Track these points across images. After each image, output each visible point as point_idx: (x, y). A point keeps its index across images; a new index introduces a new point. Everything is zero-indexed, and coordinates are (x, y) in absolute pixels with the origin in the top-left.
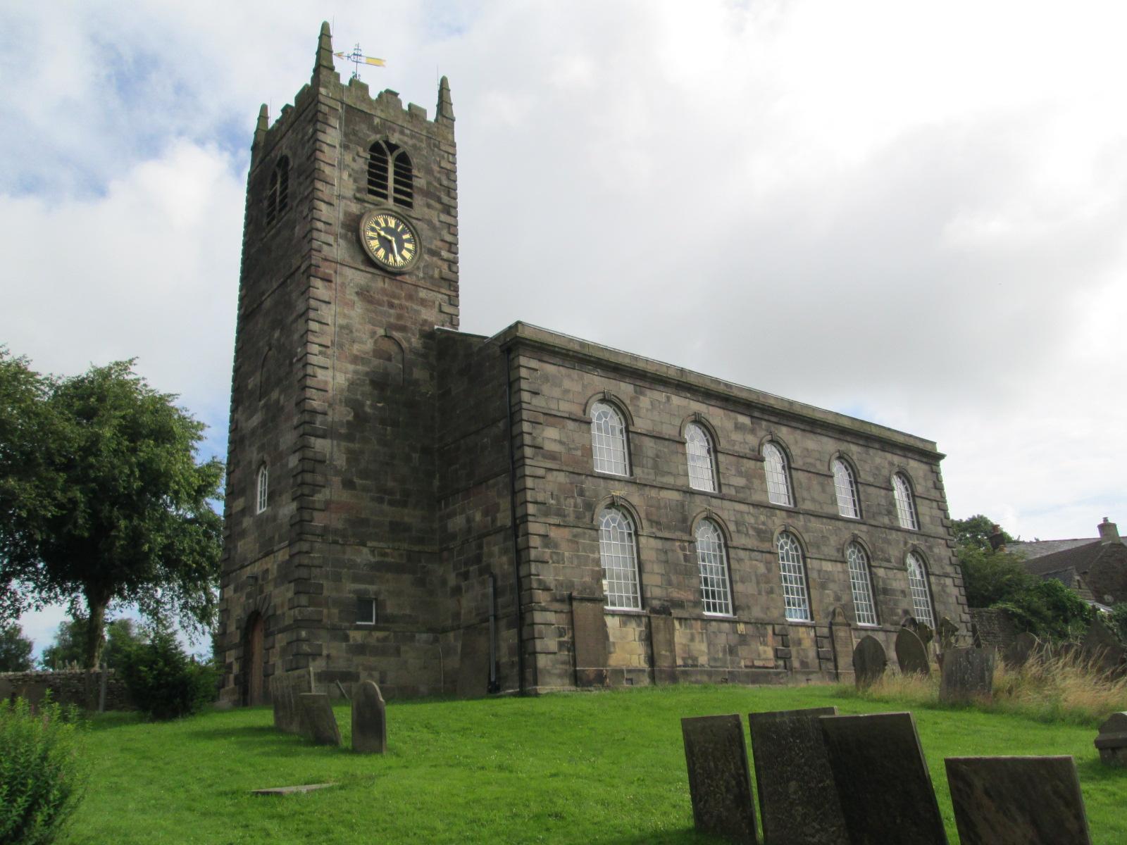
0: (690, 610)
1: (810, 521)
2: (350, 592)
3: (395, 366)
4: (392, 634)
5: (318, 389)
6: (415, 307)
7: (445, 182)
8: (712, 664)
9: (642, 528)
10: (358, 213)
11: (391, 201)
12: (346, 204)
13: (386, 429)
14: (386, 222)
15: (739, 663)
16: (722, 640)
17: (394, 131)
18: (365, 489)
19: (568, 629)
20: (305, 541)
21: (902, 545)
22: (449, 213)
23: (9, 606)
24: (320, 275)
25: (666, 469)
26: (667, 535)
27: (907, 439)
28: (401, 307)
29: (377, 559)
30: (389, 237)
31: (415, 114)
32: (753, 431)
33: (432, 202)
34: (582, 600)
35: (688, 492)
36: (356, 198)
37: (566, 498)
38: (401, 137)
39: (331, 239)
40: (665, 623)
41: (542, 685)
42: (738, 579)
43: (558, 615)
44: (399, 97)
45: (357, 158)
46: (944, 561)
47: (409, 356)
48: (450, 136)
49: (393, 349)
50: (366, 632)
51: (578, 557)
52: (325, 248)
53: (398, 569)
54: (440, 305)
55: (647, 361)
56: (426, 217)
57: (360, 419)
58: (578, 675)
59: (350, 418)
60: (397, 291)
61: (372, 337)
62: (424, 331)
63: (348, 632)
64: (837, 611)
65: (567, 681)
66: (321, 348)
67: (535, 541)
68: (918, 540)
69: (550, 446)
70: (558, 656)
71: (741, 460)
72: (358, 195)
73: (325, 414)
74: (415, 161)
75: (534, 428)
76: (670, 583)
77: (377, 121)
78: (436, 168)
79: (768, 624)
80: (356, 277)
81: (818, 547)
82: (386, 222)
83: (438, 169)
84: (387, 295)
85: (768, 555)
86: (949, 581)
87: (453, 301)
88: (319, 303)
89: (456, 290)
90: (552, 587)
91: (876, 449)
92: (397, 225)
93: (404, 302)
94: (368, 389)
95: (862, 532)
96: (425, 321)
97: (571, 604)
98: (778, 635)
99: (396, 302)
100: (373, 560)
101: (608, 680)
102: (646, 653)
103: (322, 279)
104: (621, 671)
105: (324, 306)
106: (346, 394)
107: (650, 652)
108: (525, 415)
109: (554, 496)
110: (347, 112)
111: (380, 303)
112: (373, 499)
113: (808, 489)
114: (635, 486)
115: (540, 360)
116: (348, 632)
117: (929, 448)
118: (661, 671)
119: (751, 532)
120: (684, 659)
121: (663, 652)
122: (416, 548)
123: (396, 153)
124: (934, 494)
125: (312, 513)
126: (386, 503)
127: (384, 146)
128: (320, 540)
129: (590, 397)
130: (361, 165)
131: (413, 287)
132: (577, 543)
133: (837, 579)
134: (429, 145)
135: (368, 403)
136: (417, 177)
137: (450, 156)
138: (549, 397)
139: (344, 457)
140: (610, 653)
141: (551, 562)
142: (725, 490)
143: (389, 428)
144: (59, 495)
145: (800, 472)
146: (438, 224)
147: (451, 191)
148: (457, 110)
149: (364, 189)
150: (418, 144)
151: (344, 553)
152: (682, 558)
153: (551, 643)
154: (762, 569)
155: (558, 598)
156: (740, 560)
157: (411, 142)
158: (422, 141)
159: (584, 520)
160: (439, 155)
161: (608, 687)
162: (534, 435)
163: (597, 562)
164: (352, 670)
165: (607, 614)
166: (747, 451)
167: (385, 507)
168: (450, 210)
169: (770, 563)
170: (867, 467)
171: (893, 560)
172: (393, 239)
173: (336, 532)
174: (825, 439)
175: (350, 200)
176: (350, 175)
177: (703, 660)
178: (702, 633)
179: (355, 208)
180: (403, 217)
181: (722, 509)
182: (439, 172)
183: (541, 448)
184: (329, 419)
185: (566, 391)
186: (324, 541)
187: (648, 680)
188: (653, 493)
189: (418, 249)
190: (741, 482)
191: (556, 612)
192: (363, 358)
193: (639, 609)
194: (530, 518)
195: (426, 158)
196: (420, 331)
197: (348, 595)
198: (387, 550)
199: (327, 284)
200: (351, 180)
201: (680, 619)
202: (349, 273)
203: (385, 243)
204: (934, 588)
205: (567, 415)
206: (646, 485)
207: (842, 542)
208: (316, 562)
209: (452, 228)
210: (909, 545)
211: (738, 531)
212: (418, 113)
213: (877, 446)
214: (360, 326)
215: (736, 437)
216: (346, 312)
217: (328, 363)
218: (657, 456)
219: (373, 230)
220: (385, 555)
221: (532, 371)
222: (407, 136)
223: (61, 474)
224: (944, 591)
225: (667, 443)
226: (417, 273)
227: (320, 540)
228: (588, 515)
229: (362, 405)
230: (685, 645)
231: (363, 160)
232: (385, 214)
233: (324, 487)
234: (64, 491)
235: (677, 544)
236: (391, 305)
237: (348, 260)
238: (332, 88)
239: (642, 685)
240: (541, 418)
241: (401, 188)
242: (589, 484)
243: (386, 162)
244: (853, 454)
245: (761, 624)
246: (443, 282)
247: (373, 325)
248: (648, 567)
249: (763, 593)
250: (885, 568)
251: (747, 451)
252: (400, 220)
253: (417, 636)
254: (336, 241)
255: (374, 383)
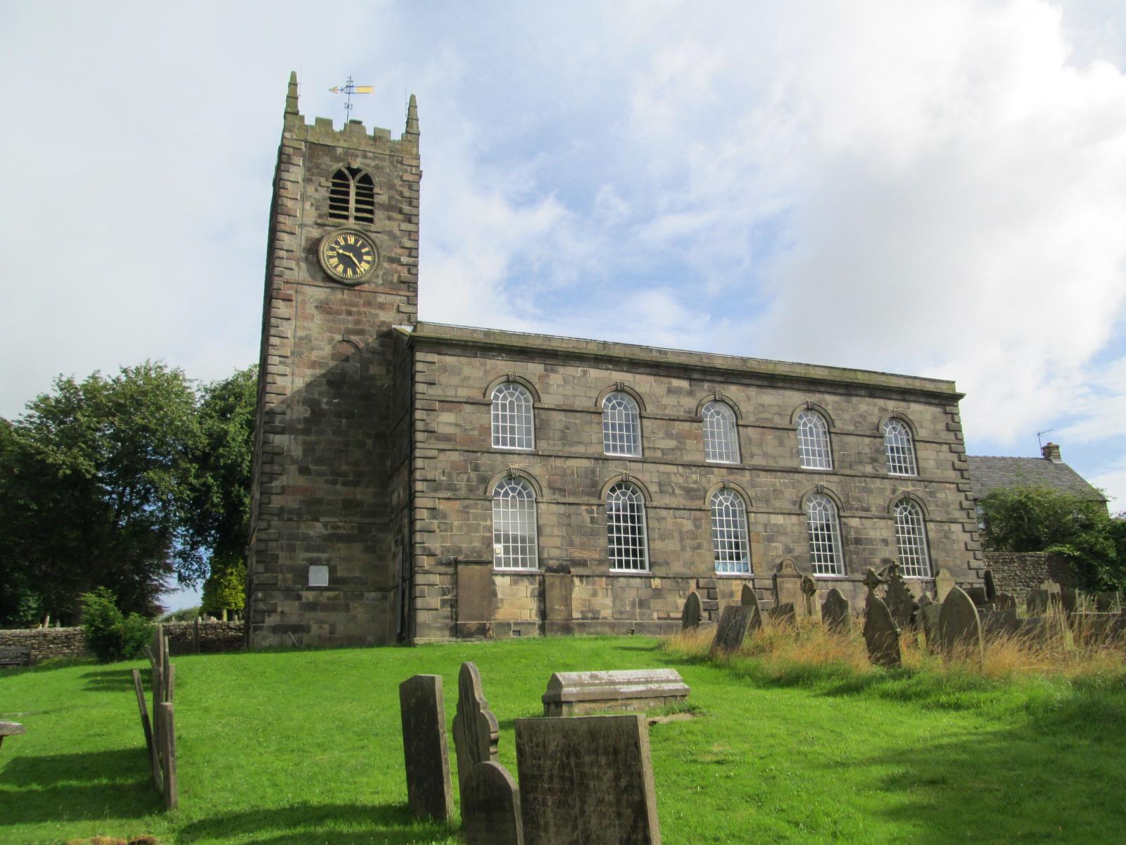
0: (594, 568)
1: (758, 476)
2: (303, 560)
3: (354, 365)
4: (342, 594)
5: (277, 394)
6: (373, 311)
7: (407, 193)
8: (618, 617)
9: (542, 496)
10: (319, 237)
11: (352, 221)
12: (308, 231)
13: (341, 422)
14: (346, 240)
15: (652, 615)
16: (631, 595)
17: (357, 156)
18: (321, 474)
19: (453, 588)
20: (263, 520)
21: (888, 493)
22: (410, 221)
23: (196, 569)
24: (280, 296)
25: (575, 439)
26: (571, 500)
27: (910, 381)
28: (359, 313)
29: (330, 531)
30: (347, 254)
31: (379, 137)
32: (691, 393)
33: (394, 215)
34: (467, 563)
35: (601, 459)
36: (317, 224)
37: (458, 475)
38: (363, 161)
39: (293, 264)
40: (561, 581)
41: (421, 636)
42: (656, 536)
43: (442, 577)
44: (363, 124)
45: (319, 188)
46: (952, 506)
47: (366, 355)
48: (414, 151)
49: (351, 350)
50: (318, 593)
51: (468, 525)
52: (287, 272)
53: (349, 539)
54: (398, 306)
55: (562, 339)
56: (387, 229)
57: (317, 414)
58: (459, 628)
59: (307, 415)
60: (356, 300)
61: (330, 343)
62: (382, 331)
63: (300, 592)
64: (785, 563)
65: (447, 633)
66: (281, 359)
67: (422, 514)
68: (913, 486)
69: (443, 430)
70: (440, 612)
71: (672, 422)
72: (319, 221)
73: (284, 413)
74: (376, 180)
75: (428, 415)
76: (571, 544)
77: (339, 151)
78: (398, 182)
79: (692, 578)
80: (318, 293)
81: (767, 501)
82: (346, 240)
83: (401, 183)
84: (346, 305)
85: (698, 513)
86: (956, 528)
87: (412, 301)
88: (280, 321)
89: (415, 291)
90: (438, 552)
91: (862, 396)
92: (356, 241)
93: (362, 309)
94: (324, 388)
95: (832, 484)
96: (383, 323)
97: (456, 568)
98: (702, 588)
99: (354, 309)
100: (325, 532)
101: (491, 632)
102: (539, 607)
103: (284, 300)
104: (509, 625)
105: (284, 322)
106: (304, 394)
107: (542, 607)
108: (418, 404)
109: (446, 474)
110: (310, 148)
111: (339, 313)
112: (327, 482)
113: (760, 444)
114: (538, 458)
115: (439, 354)
116: (300, 592)
117: (945, 389)
118: (552, 624)
119: (678, 491)
120: (582, 612)
121: (557, 607)
122: (367, 521)
123: (358, 177)
124: (950, 437)
125: (270, 498)
126: (339, 485)
127: (346, 172)
128: (276, 518)
129: (492, 381)
130: (324, 193)
131: (371, 294)
132: (468, 513)
133: (789, 531)
134: (392, 163)
135: (325, 400)
136: (378, 194)
137: (414, 169)
138: (446, 386)
139: (301, 448)
140: (498, 608)
141: (438, 531)
142: (647, 454)
143: (344, 420)
144: (194, 481)
145: (750, 428)
146: (398, 233)
147: (413, 201)
148: (423, 126)
149: (325, 215)
150: (381, 164)
151: (298, 528)
152: (588, 520)
153: (435, 602)
154: (688, 525)
155: (444, 562)
156: (660, 519)
157: (373, 164)
158: (385, 161)
159: (478, 492)
160: (401, 170)
161: (491, 638)
162: (428, 421)
163: (489, 529)
164: (304, 623)
165: (497, 575)
166: (683, 414)
167: (339, 487)
168: (411, 218)
169: (700, 519)
170: (847, 416)
171: (873, 509)
172: (351, 255)
173: (291, 511)
174: (788, 393)
175: (311, 226)
176: (312, 205)
177: (607, 613)
178: (607, 589)
179: (316, 233)
180: (362, 233)
181: (643, 471)
182: (402, 186)
183: (434, 432)
184: (288, 417)
185: (466, 379)
186: (280, 519)
187: (538, 631)
188: (559, 462)
189: (377, 259)
190: (671, 444)
191: (440, 574)
192: (320, 363)
193: (535, 569)
194: (418, 494)
195: (389, 175)
196: (377, 331)
197: (301, 563)
198: (339, 524)
199: (288, 303)
200: (313, 209)
201: (581, 577)
202: (309, 291)
203: (344, 260)
204: (931, 535)
205: (465, 400)
206: (550, 456)
207: (801, 495)
208: (273, 537)
209: (413, 235)
210: (899, 493)
211: (661, 492)
212: (381, 135)
213: (863, 392)
214: (319, 336)
215: (670, 401)
216: (305, 324)
217: (288, 370)
218: (567, 428)
219: (332, 249)
220: (338, 527)
221: (429, 364)
222: (370, 158)
223: (194, 465)
224: (948, 538)
225: (579, 414)
226: (376, 280)
227: (276, 518)
228: (482, 487)
229: (318, 403)
230: (585, 600)
231: (325, 189)
232: (345, 234)
233: (281, 474)
234: (197, 477)
235: (584, 508)
236: (350, 313)
237: (309, 279)
238: (296, 131)
239: (531, 636)
240: (437, 405)
241: (342, 213)
242: (484, 460)
243: (348, 186)
244: (827, 405)
245: (682, 578)
246: (402, 285)
247: (331, 332)
248: (547, 531)
249: (688, 549)
250: (861, 518)
251: (682, 413)
252: (360, 236)
253: (366, 594)
254: (298, 264)
255: (331, 383)
